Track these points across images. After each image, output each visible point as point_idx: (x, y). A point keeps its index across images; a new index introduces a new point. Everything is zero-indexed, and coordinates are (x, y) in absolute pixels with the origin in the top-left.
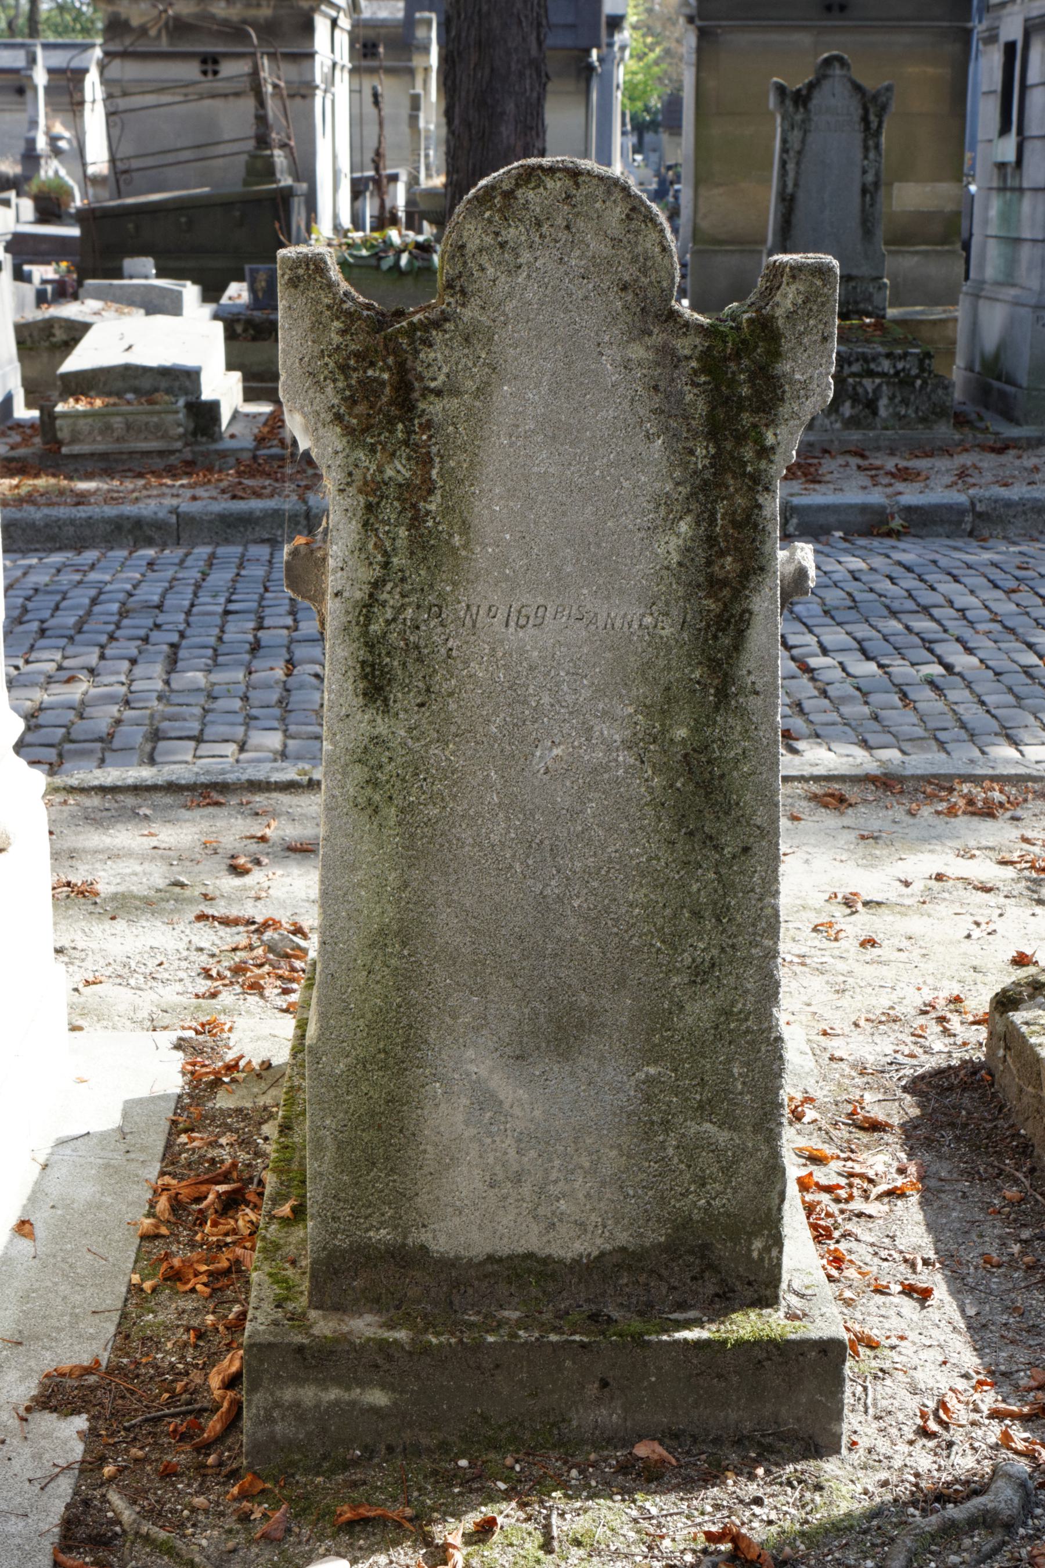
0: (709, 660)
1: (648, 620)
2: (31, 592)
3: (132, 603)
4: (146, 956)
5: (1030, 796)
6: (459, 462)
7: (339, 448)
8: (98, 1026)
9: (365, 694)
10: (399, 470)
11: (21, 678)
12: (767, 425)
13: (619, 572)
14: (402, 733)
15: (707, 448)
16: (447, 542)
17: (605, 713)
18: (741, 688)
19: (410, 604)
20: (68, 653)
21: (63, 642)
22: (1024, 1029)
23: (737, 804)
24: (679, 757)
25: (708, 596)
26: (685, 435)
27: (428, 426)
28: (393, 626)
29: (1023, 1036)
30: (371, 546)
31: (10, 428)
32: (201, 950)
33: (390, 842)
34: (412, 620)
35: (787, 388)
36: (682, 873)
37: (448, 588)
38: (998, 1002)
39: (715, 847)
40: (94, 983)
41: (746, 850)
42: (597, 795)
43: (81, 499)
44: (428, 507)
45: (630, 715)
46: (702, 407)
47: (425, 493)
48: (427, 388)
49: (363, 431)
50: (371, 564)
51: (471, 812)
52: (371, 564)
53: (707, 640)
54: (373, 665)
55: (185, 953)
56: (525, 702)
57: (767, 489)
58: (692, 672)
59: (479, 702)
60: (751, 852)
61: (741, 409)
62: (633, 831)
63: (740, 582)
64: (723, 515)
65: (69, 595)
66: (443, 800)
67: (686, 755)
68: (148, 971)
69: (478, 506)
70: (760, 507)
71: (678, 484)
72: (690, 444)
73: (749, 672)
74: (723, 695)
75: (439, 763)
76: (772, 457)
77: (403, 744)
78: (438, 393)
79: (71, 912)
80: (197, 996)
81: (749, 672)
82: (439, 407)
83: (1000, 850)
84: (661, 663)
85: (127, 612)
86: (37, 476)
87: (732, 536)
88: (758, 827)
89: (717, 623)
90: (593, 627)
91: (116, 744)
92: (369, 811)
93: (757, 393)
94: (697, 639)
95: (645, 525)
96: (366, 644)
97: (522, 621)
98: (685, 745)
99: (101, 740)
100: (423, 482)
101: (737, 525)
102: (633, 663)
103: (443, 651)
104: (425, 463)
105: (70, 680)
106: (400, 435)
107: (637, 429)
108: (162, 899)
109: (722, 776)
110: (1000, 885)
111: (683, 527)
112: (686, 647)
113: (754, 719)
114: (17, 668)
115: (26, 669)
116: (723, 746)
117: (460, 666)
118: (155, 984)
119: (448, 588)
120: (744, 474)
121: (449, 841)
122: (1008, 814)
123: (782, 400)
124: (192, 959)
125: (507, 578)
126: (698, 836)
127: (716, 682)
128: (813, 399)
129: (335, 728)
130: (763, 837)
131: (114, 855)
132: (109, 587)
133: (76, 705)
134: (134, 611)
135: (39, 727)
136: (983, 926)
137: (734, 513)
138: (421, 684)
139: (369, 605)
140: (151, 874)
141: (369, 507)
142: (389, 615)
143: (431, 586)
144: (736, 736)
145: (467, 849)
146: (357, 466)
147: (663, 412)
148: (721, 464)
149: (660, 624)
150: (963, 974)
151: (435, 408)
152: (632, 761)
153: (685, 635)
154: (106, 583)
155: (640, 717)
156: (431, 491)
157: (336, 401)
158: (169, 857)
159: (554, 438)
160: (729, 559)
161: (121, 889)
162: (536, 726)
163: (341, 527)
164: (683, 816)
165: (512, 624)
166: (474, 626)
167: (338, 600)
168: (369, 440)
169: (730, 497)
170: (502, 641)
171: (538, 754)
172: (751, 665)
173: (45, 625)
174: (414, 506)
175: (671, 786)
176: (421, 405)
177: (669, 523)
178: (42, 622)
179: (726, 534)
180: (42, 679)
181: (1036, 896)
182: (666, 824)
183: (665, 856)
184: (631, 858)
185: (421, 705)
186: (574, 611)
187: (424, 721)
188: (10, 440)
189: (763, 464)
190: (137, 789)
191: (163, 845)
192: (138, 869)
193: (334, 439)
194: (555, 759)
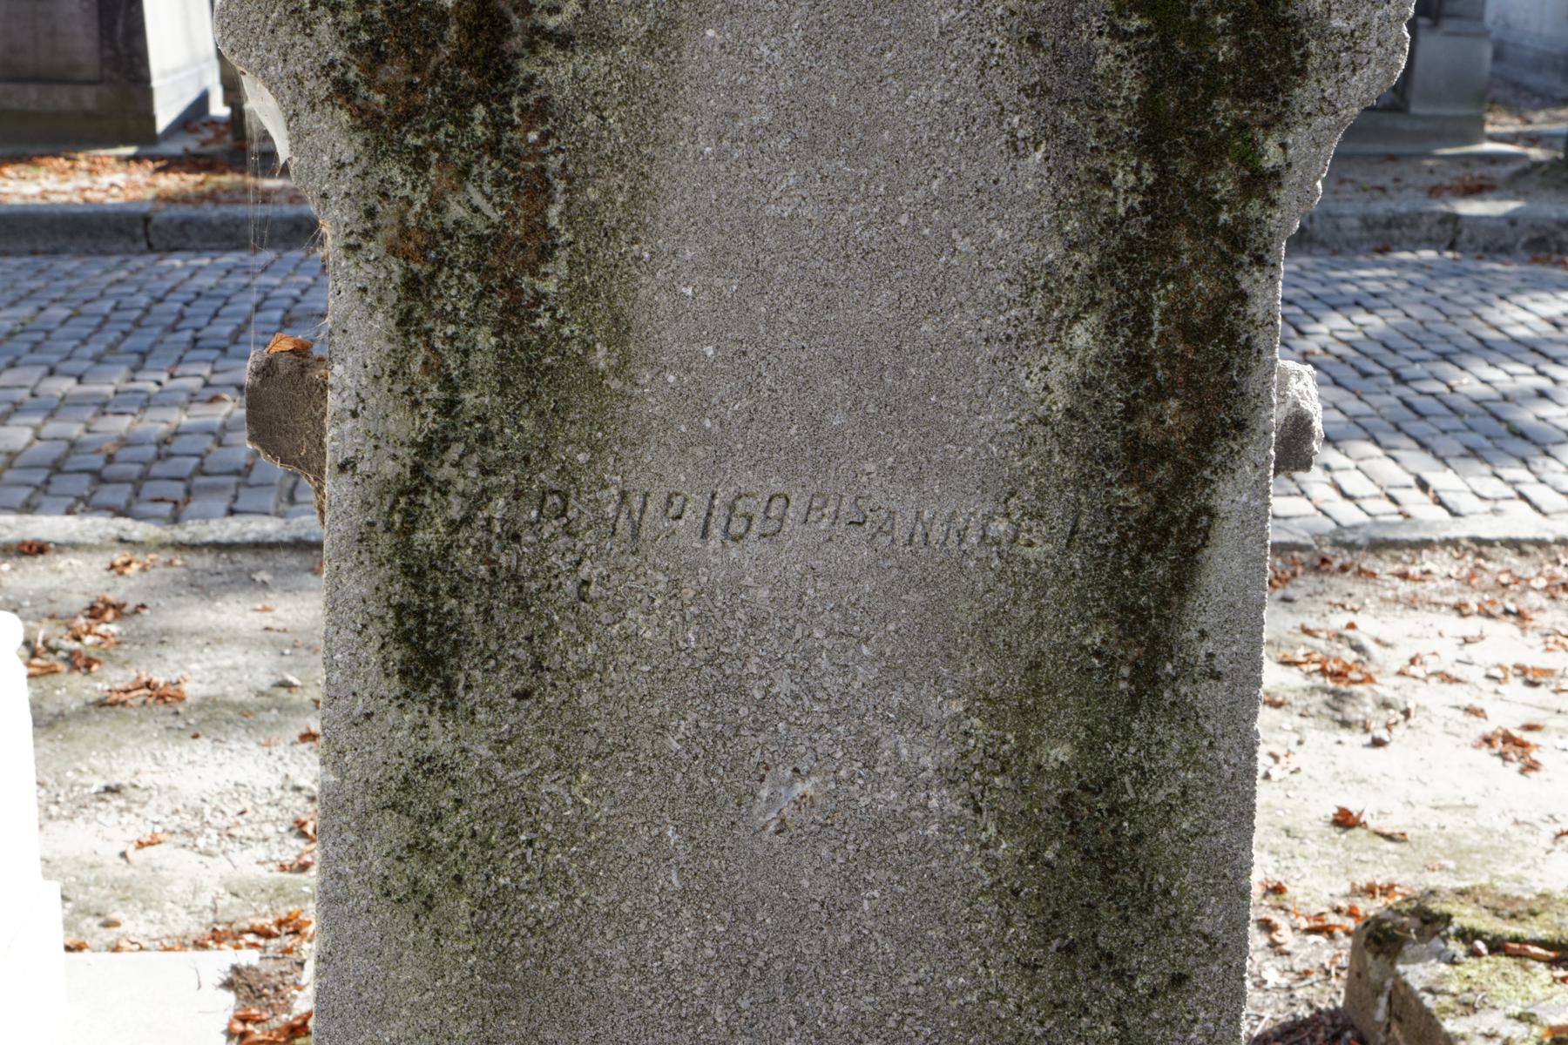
0: (1123, 608)
1: (1000, 527)
2: (192, 296)
3: (297, 310)
4: (227, 798)
5: (1300, 570)
6: (607, 192)
7: (347, 156)
8: (142, 917)
9: (404, 674)
10: (475, 205)
11: (161, 396)
12: (1267, 126)
13: (942, 428)
14: (483, 750)
15: (1137, 171)
16: (580, 361)
17: (904, 712)
18: (1185, 668)
19: (500, 488)
20: (219, 366)
21: (214, 354)
22: (1428, 1000)
23: (1166, 893)
24: (1053, 801)
25: (1125, 481)
26: (1093, 142)
27: (540, 111)
28: (463, 533)
29: (1428, 1014)
30: (416, 367)
31: (205, 125)
32: (298, 789)
33: (457, 966)
34: (504, 521)
35: (1313, 45)
36: (1049, 1024)
37: (581, 457)
38: (1369, 936)
39: (1119, 976)
40: (150, 844)
41: (1179, 980)
42: (883, 875)
43: (266, 197)
44: (541, 286)
45: (956, 718)
46: (1131, 84)
47: (532, 257)
48: (538, 30)
49: (399, 121)
50: (416, 404)
51: (625, 908)
52: (416, 404)
53: (1118, 570)
54: (420, 614)
55: (278, 794)
56: (741, 691)
57: (1259, 261)
58: (1086, 632)
59: (644, 689)
60: (1188, 985)
61: (1213, 90)
62: (952, 945)
63: (1195, 452)
64: (1165, 312)
65: (233, 300)
66: (567, 883)
67: (1066, 798)
68: (225, 824)
69: (647, 287)
70: (1243, 297)
71: (1073, 246)
72: (1102, 163)
73: (1203, 634)
74: (1147, 678)
75: (558, 810)
76: (1274, 194)
77: (485, 774)
78: (564, 41)
79: (143, 726)
80: (283, 868)
81: (1203, 634)
82: (564, 72)
83: (1279, 645)
84: (1024, 614)
85: (291, 320)
86: (223, 173)
87: (1182, 356)
88: (1206, 937)
89: (1143, 535)
90: (884, 541)
91: (255, 477)
92: (414, 905)
93: (1250, 55)
94: (1099, 566)
95: (1001, 331)
96: (406, 570)
97: (737, 527)
98: (1065, 779)
99: (237, 473)
100: (530, 232)
101: (1193, 335)
102: (966, 612)
103: (570, 586)
104: (533, 193)
105: (215, 399)
106: (479, 130)
107: (993, 129)
108: (262, 708)
109: (1138, 839)
110: (1290, 697)
111: (1081, 336)
112: (1077, 583)
113: (1208, 727)
114: (159, 383)
115: (169, 384)
116: (1144, 777)
117: (605, 617)
118: (230, 846)
119: (581, 457)
120: (1213, 229)
121: (579, 964)
122: (1279, 593)
123: (1302, 72)
124: (286, 803)
125: (707, 438)
126: (1084, 955)
127: (1135, 652)
128: (1367, 72)
129: (342, 738)
130: (1214, 957)
131: (215, 639)
132: (276, 293)
133: (216, 429)
134: (298, 319)
135: (170, 455)
136: (1283, 760)
137: (1189, 308)
138: (522, 653)
139: (411, 492)
140: (255, 668)
141: (412, 285)
142: (455, 512)
143: (546, 452)
144: (1170, 760)
145: (615, 978)
146: (385, 195)
147: (1047, 91)
148: (1160, 204)
149: (1024, 536)
150: (1275, 840)
151: (555, 73)
152: (956, 808)
153: (1076, 559)
154: (273, 288)
155: (977, 722)
156: (546, 254)
157: (338, 54)
158: (282, 643)
159: (813, 143)
160: (1174, 404)
161: (214, 691)
162: (762, 738)
163: (351, 325)
164: (1056, 915)
165: (716, 532)
166: (635, 536)
167: (346, 478)
168: (412, 140)
169: (1181, 276)
170: (693, 568)
171: (764, 793)
172: (1208, 620)
173: (200, 335)
174: (509, 283)
175: (1034, 858)
176: (526, 67)
177: (1051, 327)
178: (197, 330)
179: (1169, 354)
180: (183, 397)
181: (1338, 716)
182: (1021, 930)
183: (1016, 990)
184: (948, 995)
185: (523, 695)
186: (845, 507)
187: (529, 727)
188: (202, 137)
189: (1254, 209)
190: (259, 547)
191: (280, 625)
192: (241, 660)
193: (336, 137)
194: (801, 802)
